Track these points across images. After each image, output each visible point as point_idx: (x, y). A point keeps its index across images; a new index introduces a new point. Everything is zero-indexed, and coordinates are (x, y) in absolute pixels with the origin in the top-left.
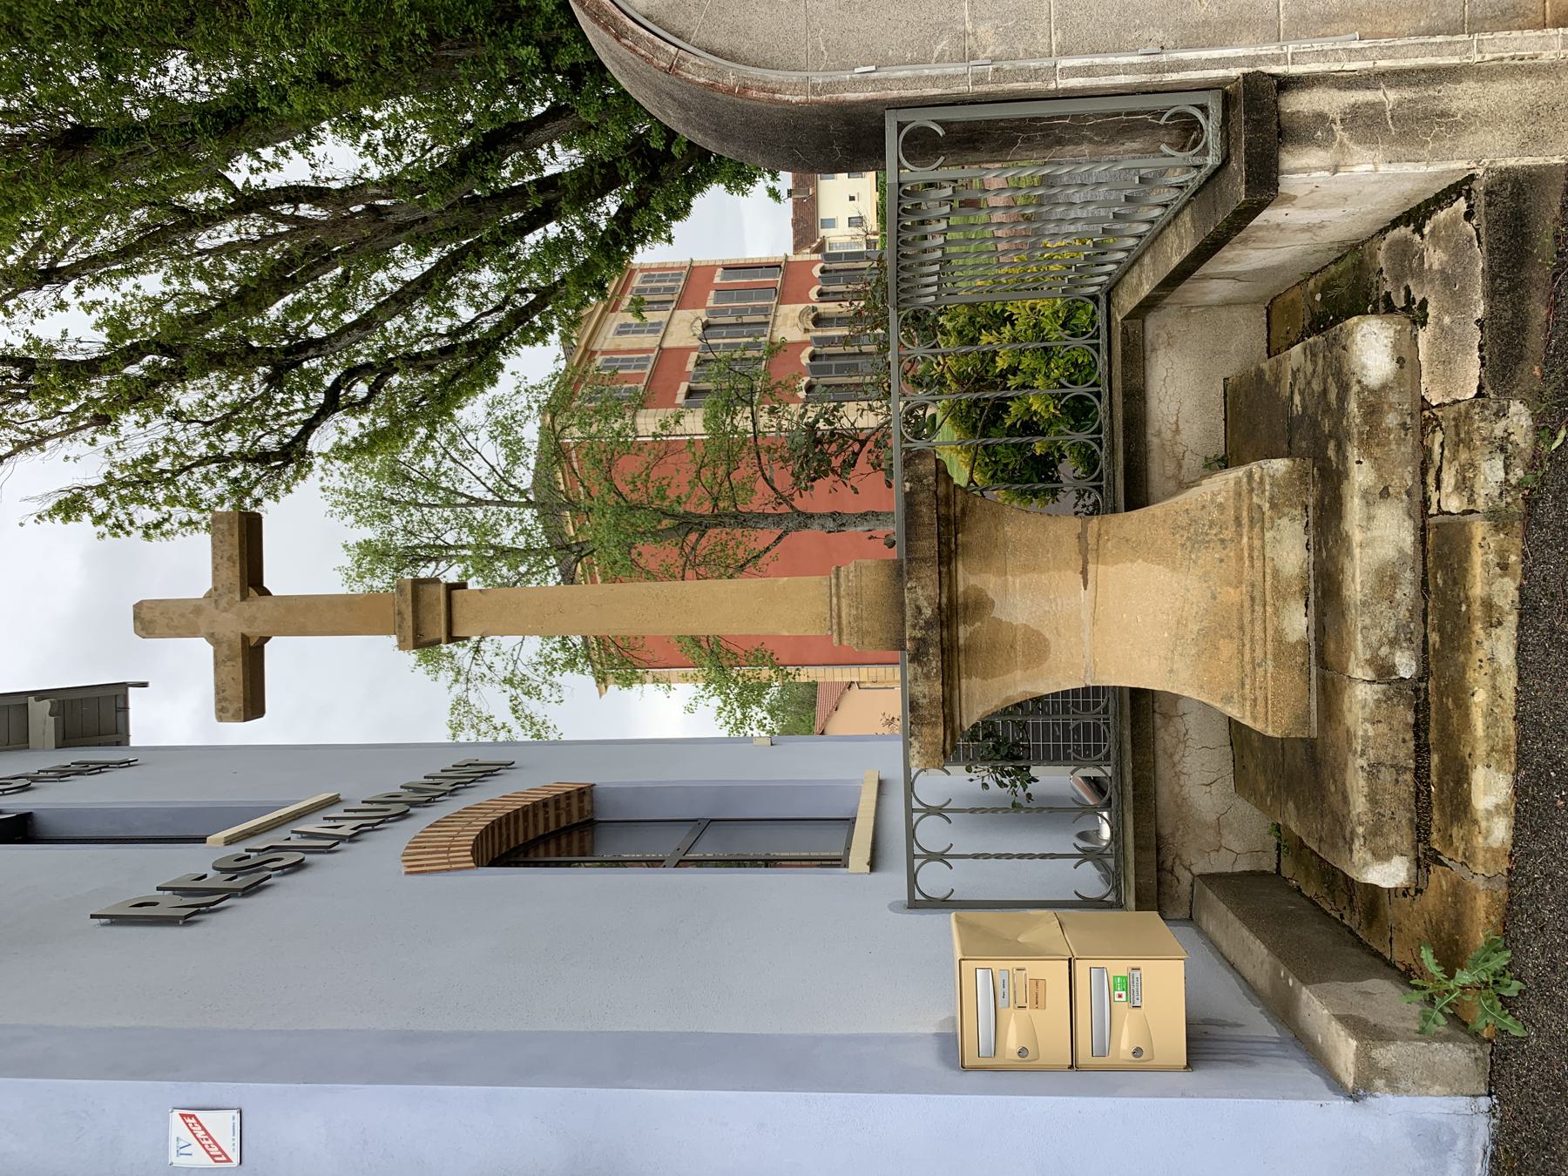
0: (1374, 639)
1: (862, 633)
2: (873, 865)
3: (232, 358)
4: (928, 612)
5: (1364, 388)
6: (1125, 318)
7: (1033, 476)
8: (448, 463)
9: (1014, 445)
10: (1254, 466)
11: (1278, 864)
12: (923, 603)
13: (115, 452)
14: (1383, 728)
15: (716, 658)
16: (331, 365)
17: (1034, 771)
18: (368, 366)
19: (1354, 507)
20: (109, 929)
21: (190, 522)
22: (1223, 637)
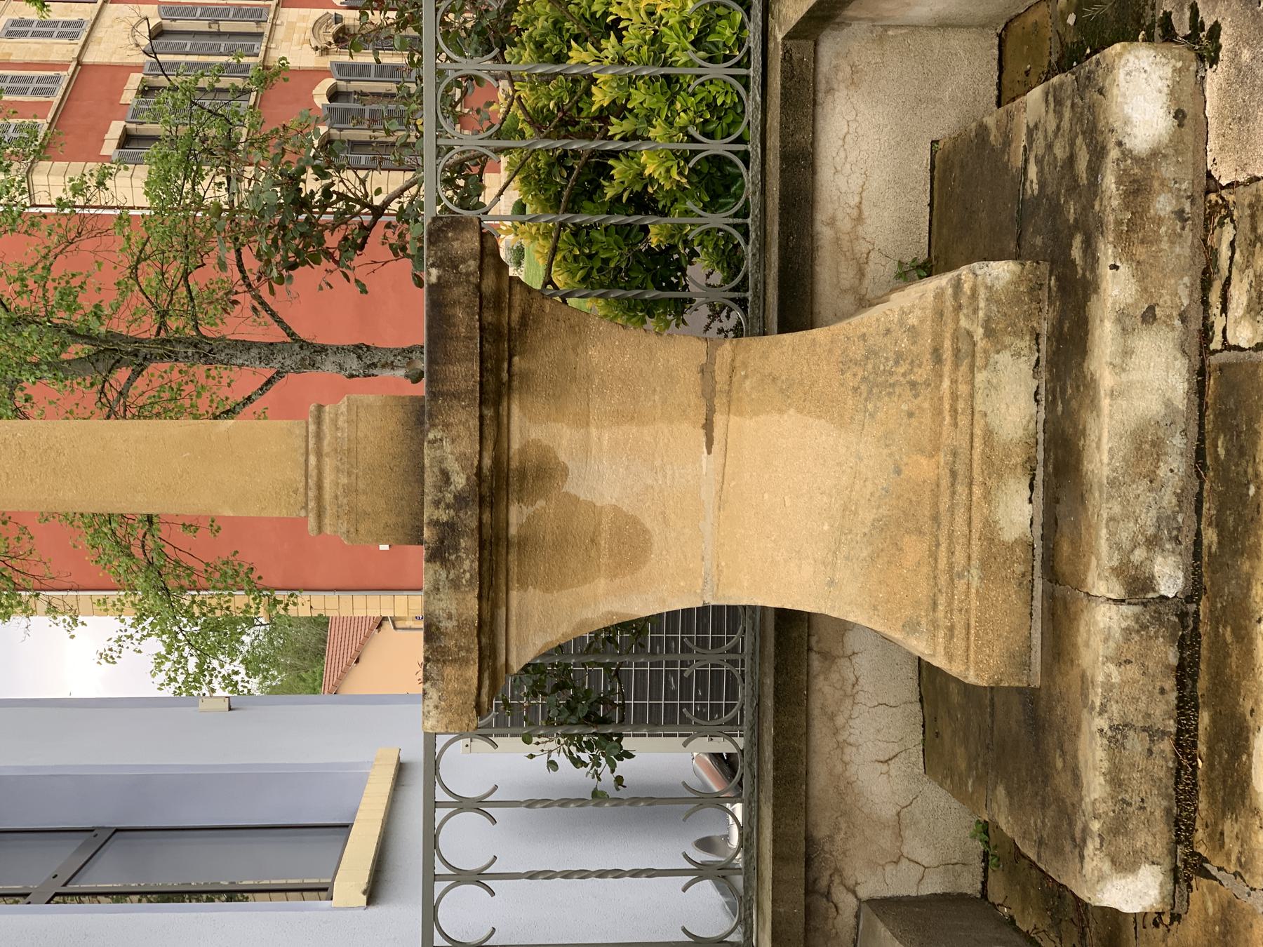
0: (1124, 537)
1: (356, 516)
2: (373, 894)
4: (459, 481)
5: (1126, 154)
6: (788, 37)
7: (646, 283)
9: (619, 228)
10: (964, 271)
11: (984, 884)
12: (453, 465)
14: (1133, 671)
15: (152, 564)
17: (627, 744)
19: (1105, 335)
22: (908, 532)
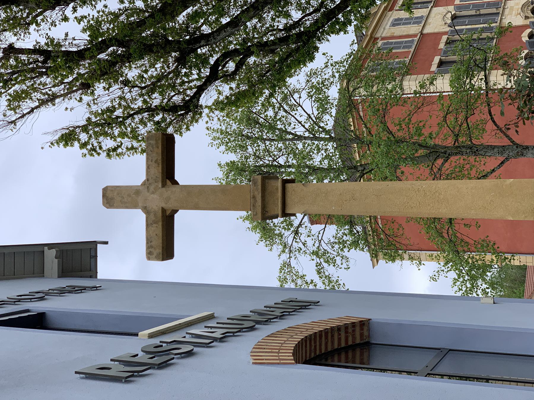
3: (155, 48)
8: (282, 113)
13: (92, 105)
16: (213, 50)
18: (236, 50)
20: (84, 381)
21: (132, 148)
